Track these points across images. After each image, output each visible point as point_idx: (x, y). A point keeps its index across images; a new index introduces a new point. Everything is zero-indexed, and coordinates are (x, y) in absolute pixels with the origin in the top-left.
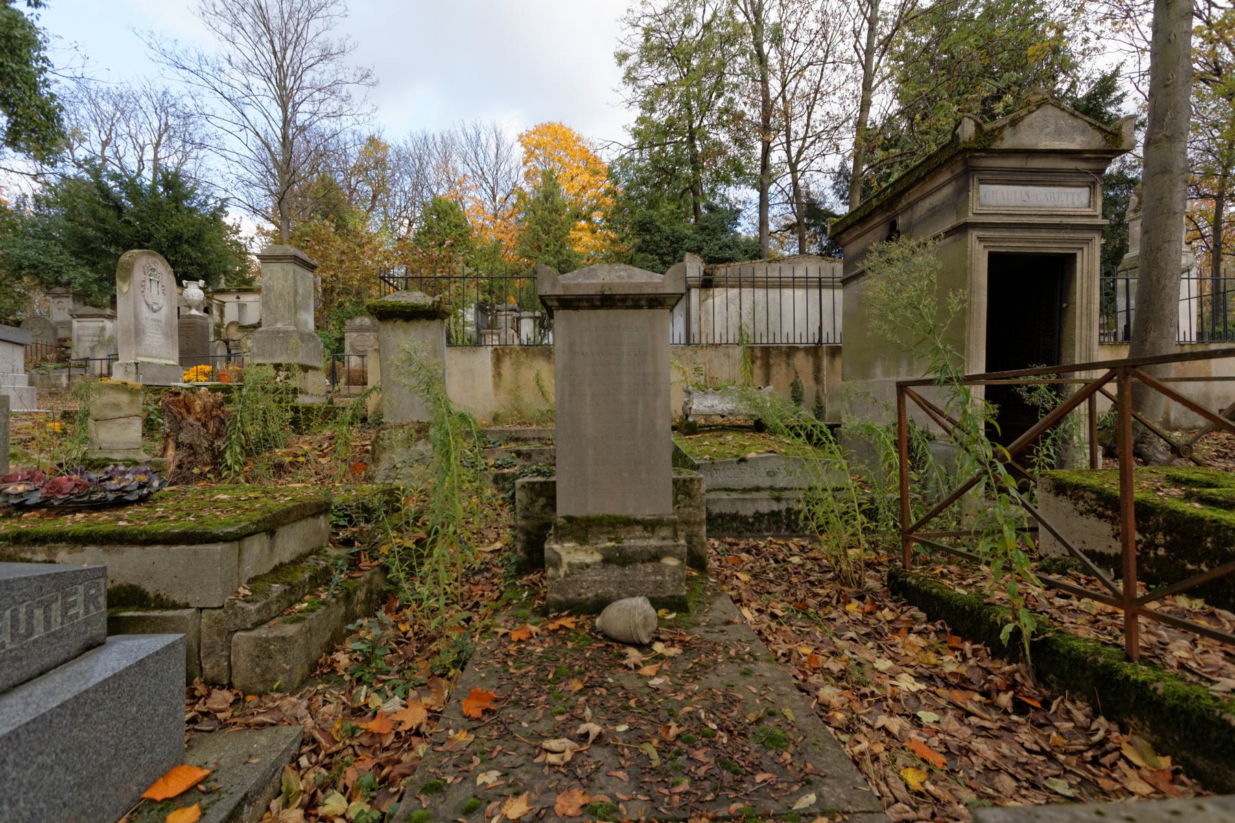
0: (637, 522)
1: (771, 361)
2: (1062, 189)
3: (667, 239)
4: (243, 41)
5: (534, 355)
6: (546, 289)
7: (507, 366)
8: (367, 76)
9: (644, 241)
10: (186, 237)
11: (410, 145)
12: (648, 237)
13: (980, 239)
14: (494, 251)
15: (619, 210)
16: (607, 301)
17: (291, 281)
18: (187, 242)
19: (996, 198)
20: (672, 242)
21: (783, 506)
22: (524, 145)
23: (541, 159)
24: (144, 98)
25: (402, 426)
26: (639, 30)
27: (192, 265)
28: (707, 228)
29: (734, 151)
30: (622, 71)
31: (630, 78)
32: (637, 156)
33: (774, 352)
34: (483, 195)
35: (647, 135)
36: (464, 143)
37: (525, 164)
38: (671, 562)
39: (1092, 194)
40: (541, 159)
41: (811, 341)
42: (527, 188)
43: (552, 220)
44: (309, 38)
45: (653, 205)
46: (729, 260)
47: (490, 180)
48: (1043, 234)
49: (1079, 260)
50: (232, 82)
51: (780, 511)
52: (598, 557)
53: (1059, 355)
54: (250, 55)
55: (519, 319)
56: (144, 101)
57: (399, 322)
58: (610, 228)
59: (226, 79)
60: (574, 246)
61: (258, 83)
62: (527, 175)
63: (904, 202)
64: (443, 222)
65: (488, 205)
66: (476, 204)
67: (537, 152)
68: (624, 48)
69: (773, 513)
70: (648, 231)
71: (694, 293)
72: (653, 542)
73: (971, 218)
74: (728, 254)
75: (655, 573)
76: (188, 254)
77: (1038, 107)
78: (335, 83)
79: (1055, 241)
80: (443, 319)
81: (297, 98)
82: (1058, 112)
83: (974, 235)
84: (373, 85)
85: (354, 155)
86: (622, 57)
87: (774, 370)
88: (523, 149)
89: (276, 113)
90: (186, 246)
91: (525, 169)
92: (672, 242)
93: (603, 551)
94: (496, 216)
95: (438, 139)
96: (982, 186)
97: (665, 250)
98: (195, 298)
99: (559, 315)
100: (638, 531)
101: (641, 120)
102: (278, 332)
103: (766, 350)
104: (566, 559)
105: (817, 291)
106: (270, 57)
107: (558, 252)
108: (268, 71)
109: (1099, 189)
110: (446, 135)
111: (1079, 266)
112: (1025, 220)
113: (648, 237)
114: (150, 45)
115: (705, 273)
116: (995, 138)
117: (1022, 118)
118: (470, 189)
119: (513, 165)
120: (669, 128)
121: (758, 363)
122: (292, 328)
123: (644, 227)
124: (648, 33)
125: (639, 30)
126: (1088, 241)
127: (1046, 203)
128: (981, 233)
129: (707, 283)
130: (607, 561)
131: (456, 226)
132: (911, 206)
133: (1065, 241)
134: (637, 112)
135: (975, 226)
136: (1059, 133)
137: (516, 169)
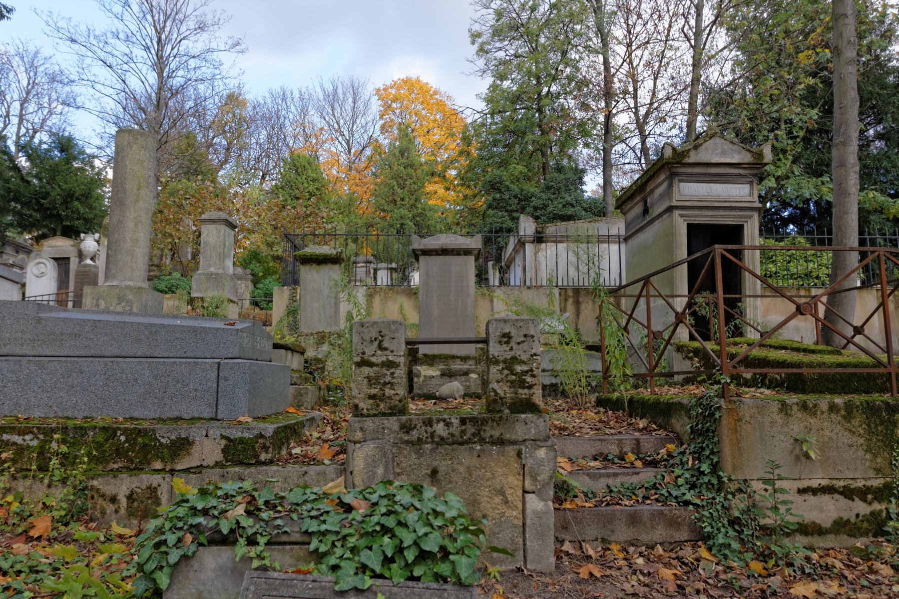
0: (458, 357)
1: (581, 300)
2: (737, 186)
3: (516, 197)
4: (129, 18)
5: (398, 293)
6: (416, 246)
7: (377, 300)
8: (237, 44)
9: (494, 199)
10: (77, 195)
11: (269, 101)
12: (498, 196)
13: (681, 216)
14: (347, 207)
15: (471, 168)
16: (444, 252)
17: (222, 238)
18: (77, 199)
19: (690, 191)
20: (520, 200)
21: (558, 381)
22: (381, 98)
23: (397, 111)
24: (17, 58)
25: (312, 334)
26: (491, 11)
27: (78, 219)
28: (552, 187)
29: (579, 115)
30: (476, 47)
31: (482, 51)
32: (489, 121)
33: (583, 292)
34: (338, 147)
35: (496, 100)
36: (321, 97)
37: (381, 118)
38: (474, 376)
39: (752, 188)
40: (397, 111)
41: (613, 284)
42: (385, 142)
43: (408, 175)
44: (188, 13)
45: (504, 164)
46: (569, 218)
47: (346, 133)
48: (721, 213)
49: (745, 228)
50: (115, 52)
51: (557, 384)
52: (438, 373)
53: (743, 290)
54: (134, 28)
55: (376, 270)
56: (16, 61)
57: (314, 266)
58: (462, 185)
59: (108, 48)
60: (430, 199)
61: (139, 53)
62: (383, 128)
63: (648, 189)
64: (300, 179)
65: (343, 157)
66: (332, 156)
67: (394, 105)
68: (476, 27)
69: (552, 385)
70: (499, 190)
71: (529, 248)
72: (465, 367)
73: (674, 203)
74: (570, 211)
75: (466, 381)
76: (77, 209)
77: (711, 138)
78: (208, 51)
79: (729, 216)
80: (340, 264)
81: (173, 66)
82: (723, 141)
83: (676, 213)
84: (242, 52)
85: (212, 106)
86: (475, 36)
87: (583, 306)
88: (380, 102)
89: (152, 78)
90: (76, 203)
91: (382, 122)
92: (520, 200)
93: (441, 370)
94: (350, 169)
95: (296, 95)
96: (681, 184)
97: (514, 207)
98: (91, 249)
99: (421, 258)
100: (458, 361)
101: (494, 87)
102: (212, 274)
103: (577, 291)
104: (423, 373)
105: (617, 246)
106: (151, 31)
107: (413, 206)
108: (148, 41)
109: (755, 185)
110: (304, 90)
111: (745, 232)
112: (708, 204)
113: (498, 196)
114: (47, 22)
115: (537, 232)
116: (684, 157)
117: (701, 145)
118: (324, 142)
119: (369, 119)
120: (516, 98)
121: (570, 301)
122: (221, 271)
123: (494, 186)
124: (499, 14)
125: (491, 11)
126: (750, 217)
127: (314, 272)
128: (681, 212)
129: (539, 239)
130: (443, 375)
131: (314, 180)
132: (652, 191)
133: (735, 217)
134: (489, 80)
135: (677, 207)
136: (724, 153)
137: (371, 125)
